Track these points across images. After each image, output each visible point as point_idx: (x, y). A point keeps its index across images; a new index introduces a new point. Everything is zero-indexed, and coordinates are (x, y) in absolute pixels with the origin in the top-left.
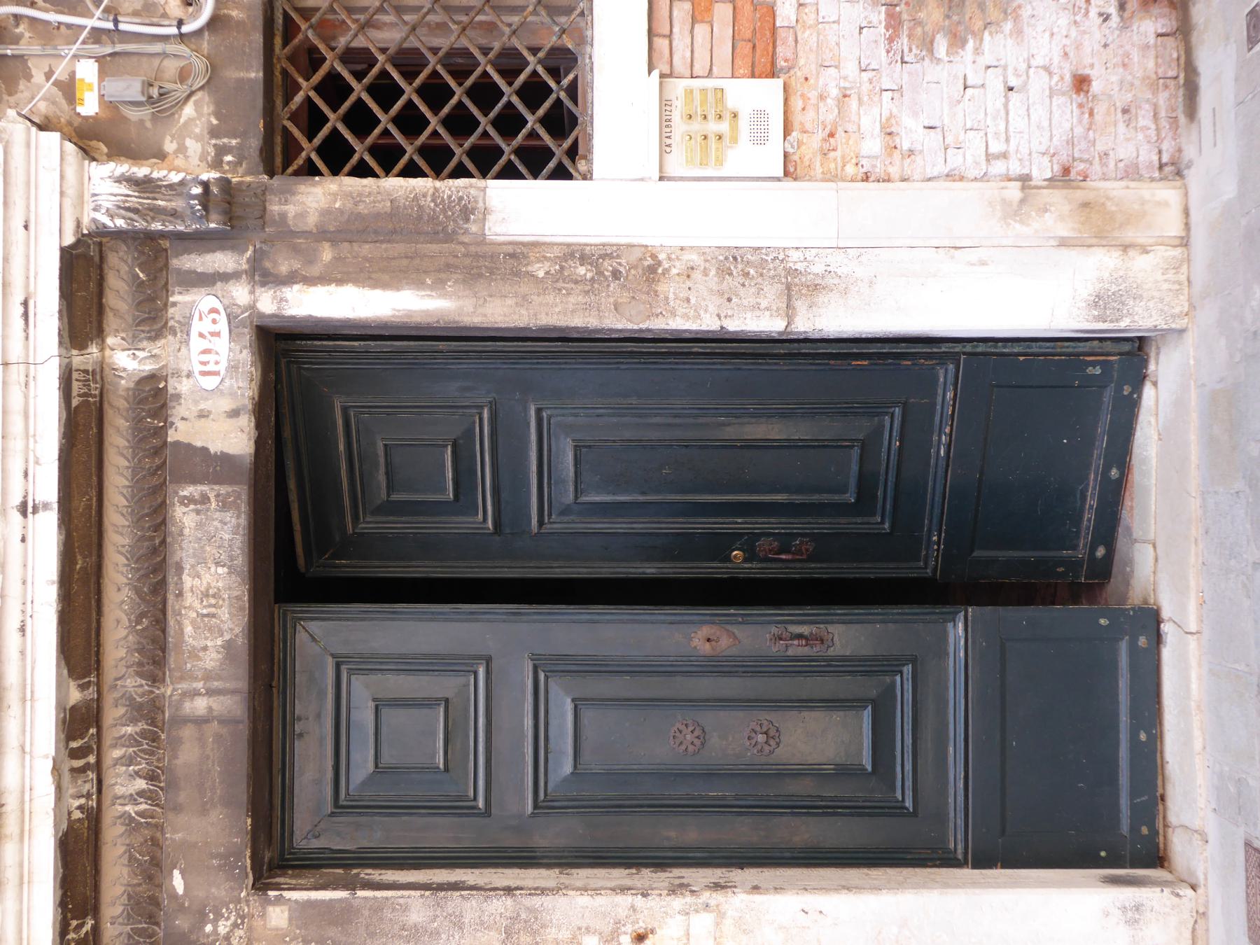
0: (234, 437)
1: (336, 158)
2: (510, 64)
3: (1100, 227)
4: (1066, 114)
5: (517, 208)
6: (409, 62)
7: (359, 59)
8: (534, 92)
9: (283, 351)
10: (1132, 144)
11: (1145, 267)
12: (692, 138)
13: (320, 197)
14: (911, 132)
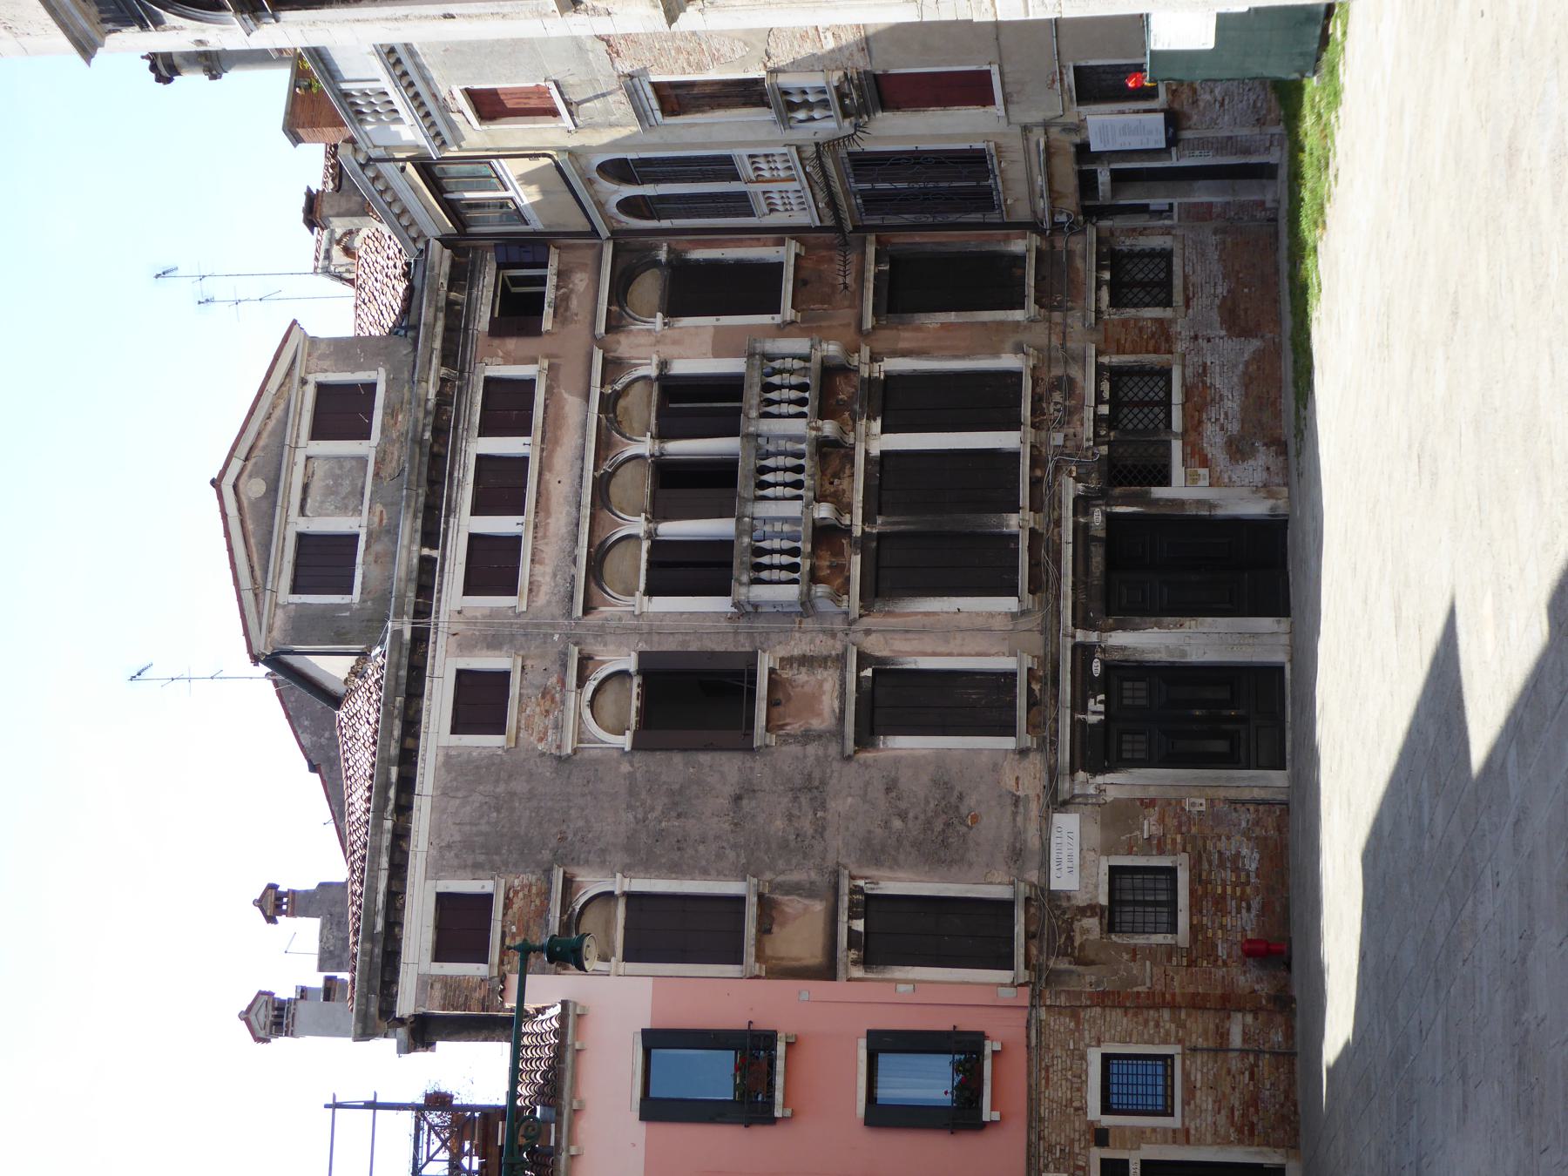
0: (1102, 534)
1: (1121, 485)
2: (1155, 466)
3: (1271, 495)
4: (1265, 475)
5: (1159, 492)
6: (1135, 466)
7: (1125, 467)
8: (1160, 472)
9: (1110, 518)
10: (1278, 480)
11: (1280, 502)
12: (1191, 480)
13: (1118, 491)
14: (1234, 478)
